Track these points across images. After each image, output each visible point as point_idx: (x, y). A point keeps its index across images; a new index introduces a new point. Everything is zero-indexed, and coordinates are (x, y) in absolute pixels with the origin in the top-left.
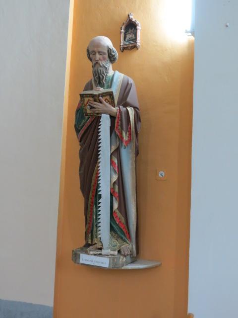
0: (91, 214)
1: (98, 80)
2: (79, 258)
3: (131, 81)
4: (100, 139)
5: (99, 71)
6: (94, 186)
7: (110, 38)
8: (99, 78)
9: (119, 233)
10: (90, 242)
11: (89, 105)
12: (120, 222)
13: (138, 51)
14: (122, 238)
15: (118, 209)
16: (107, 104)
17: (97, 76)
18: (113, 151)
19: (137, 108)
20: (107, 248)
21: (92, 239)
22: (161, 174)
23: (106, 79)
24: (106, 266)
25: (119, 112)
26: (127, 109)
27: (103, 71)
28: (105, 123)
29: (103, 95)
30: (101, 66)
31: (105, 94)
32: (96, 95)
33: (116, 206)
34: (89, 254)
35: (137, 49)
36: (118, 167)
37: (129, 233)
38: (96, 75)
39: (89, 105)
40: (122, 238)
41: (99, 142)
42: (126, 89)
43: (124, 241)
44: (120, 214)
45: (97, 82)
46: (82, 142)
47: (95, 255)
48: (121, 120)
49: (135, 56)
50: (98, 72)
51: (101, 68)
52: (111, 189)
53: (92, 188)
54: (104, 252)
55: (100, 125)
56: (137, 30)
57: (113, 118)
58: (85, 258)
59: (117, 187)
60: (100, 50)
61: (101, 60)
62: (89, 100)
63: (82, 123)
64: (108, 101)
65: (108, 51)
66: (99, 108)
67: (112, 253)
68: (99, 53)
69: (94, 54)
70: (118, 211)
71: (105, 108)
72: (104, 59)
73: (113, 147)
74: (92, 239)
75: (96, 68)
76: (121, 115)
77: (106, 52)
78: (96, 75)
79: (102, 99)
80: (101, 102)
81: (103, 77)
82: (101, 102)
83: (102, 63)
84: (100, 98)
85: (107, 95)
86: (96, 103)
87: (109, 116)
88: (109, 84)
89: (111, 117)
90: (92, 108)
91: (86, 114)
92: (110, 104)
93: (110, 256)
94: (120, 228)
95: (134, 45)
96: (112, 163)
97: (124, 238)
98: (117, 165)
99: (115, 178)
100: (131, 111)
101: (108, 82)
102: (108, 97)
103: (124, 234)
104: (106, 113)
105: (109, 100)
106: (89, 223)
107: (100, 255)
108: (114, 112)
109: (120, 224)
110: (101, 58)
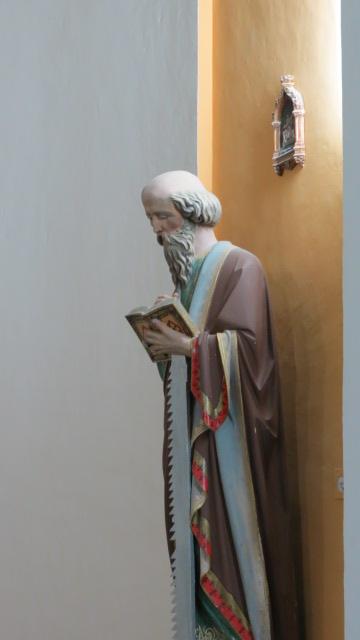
3: (249, 260)
7: (189, 171)
13: (303, 172)
15: (211, 569)
18: (195, 437)
23: (187, 270)
33: (205, 567)
36: (207, 482)
44: (220, 585)
49: (301, 181)
51: (172, 248)
56: (294, 118)
59: (206, 523)
61: (293, 152)
70: (212, 578)
72: (173, 227)
75: (197, 221)
79: (161, 325)
80: (159, 331)
81: (180, 267)
89: (188, 360)
98: (204, 470)
109: (222, 610)
110: (165, 225)
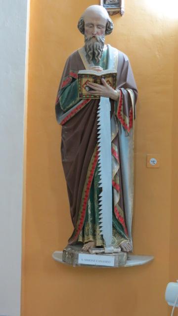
0: (84, 210)
1: (91, 56)
2: (77, 258)
3: (127, 59)
4: (99, 126)
5: (95, 46)
6: (89, 177)
8: (94, 54)
9: (118, 228)
10: (80, 240)
11: (88, 87)
12: (120, 216)
14: (120, 234)
15: (118, 203)
16: (108, 86)
17: (92, 51)
19: (136, 90)
20: (110, 246)
21: (83, 236)
22: (153, 161)
23: (101, 56)
24: (112, 264)
25: (121, 96)
26: (128, 92)
27: (99, 46)
28: (105, 107)
29: (105, 76)
30: (97, 41)
31: (108, 76)
32: (99, 76)
34: (90, 253)
35: (121, 15)
37: (126, 227)
38: (90, 50)
39: (88, 87)
40: (120, 234)
41: (98, 128)
42: (123, 66)
43: (123, 237)
45: (91, 59)
46: (71, 125)
47: (97, 254)
48: (124, 105)
50: (93, 47)
51: (98, 43)
52: (113, 181)
53: (87, 180)
54: (107, 250)
55: (99, 109)
57: (112, 101)
58: (84, 258)
60: (100, 23)
62: (88, 80)
63: (71, 105)
64: (110, 83)
65: (107, 24)
66: (100, 91)
67: (116, 250)
68: (99, 26)
69: (91, 27)
71: (107, 91)
72: (102, 32)
73: (113, 134)
74: (83, 236)
75: (91, 42)
76: (124, 99)
77: (105, 25)
78: (90, 50)
79: (104, 80)
81: (99, 54)
82: (102, 84)
83: (99, 37)
84: (103, 79)
85: (109, 77)
86: (97, 85)
87: (108, 99)
88: (105, 60)
90: (91, 89)
91: (81, 95)
92: (111, 86)
93: (114, 254)
94: (119, 223)
95: (119, 10)
96: (113, 151)
97: (123, 233)
99: (117, 168)
100: (130, 91)
101: (104, 59)
102: (110, 79)
103: (122, 229)
104: (105, 96)
105: (111, 81)
106: (81, 219)
107: (103, 253)
108: (116, 96)
109: (120, 219)
